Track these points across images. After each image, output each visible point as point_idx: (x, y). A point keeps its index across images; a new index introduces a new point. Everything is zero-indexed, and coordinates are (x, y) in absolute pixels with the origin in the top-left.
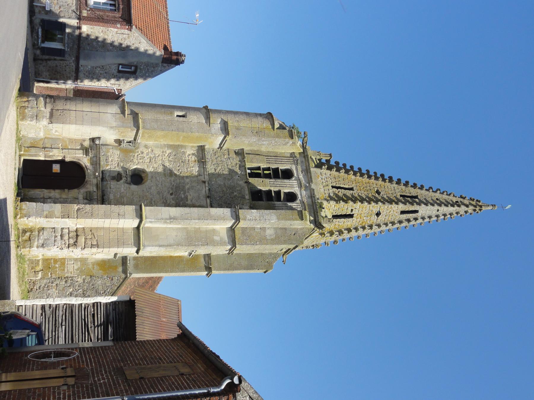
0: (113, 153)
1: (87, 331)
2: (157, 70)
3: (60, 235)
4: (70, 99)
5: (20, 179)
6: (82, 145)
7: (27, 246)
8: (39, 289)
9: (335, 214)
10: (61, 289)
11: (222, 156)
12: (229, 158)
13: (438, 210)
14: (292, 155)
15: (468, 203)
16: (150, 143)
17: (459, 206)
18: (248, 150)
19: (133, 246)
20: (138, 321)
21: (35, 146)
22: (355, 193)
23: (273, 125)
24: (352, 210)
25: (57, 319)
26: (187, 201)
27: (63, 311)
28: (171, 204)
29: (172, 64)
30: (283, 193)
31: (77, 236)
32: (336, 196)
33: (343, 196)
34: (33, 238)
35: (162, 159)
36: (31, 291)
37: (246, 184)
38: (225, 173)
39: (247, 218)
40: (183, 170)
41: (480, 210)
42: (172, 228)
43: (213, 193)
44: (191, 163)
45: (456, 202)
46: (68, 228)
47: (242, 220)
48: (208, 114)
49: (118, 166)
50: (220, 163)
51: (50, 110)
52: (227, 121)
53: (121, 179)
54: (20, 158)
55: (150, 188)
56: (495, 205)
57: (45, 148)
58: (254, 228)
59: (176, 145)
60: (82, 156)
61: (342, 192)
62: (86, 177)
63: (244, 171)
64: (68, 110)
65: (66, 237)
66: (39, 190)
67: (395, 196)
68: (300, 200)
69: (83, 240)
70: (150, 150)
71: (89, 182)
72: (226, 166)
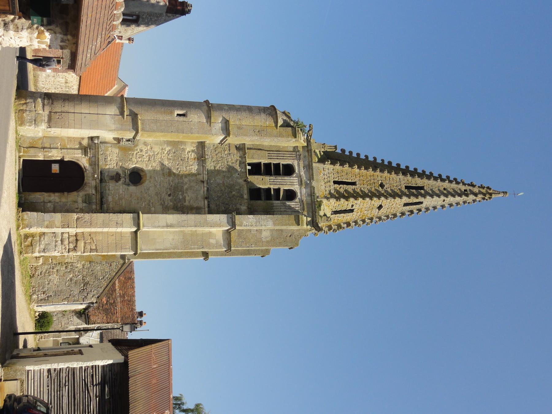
0: (111, 151)
1: (87, 390)
2: (161, 19)
3: (60, 240)
4: (68, 99)
5: (20, 181)
6: (80, 144)
7: (29, 252)
8: (41, 274)
9: (334, 210)
10: (62, 274)
11: (223, 152)
12: (230, 154)
13: (444, 201)
14: (295, 149)
15: (477, 191)
16: (150, 140)
17: (467, 195)
18: (249, 145)
19: (131, 251)
20: (131, 381)
21: (34, 146)
22: (357, 188)
23: (276, 122)
24: (352, 206)
25: (61, 380)
26: (185, 202)
27: (66, 373)
28: (169, 205)
29: (178, 14)
30: (283, 190)
31: (77, 240)
32: (337, 193)
33: (345, 192)
34: (35, 244)
35: (161, 157)
36: (33, 277)
37: (245, 183)
38: (224, 169)
39: (244, 224)
40: (182, 169)
41: (490, 198)
42: (170, 232)
43: (212, 192)
44: (190, 161)
45: (464, 190)
46: (68, 233)
47: (238, 226)
48: (209, 112)
49: (117, 166)
50: (220, 159)
51: (48, 113)
52: (228, 120)
53: (119, 179)
54: (19, 159)
55: (148, 189)
56: (506, 193)
57: (44, 148)
58: (250, 230)
59: (176, 141)
60: (81, 156)
61: (343, 188)
62: (85, 178)
63: (244, 168)
64: (67, 112)
65: (66, 242)
66: (39, 193)
67: (399, 189)
68: (299, 198)
69: (83, 244)
70: (149, 147)
71: (88, 184)
72: (226, 163)
